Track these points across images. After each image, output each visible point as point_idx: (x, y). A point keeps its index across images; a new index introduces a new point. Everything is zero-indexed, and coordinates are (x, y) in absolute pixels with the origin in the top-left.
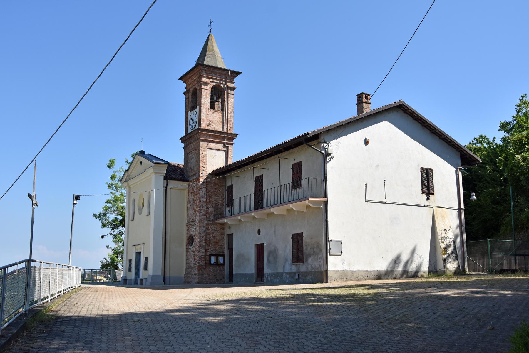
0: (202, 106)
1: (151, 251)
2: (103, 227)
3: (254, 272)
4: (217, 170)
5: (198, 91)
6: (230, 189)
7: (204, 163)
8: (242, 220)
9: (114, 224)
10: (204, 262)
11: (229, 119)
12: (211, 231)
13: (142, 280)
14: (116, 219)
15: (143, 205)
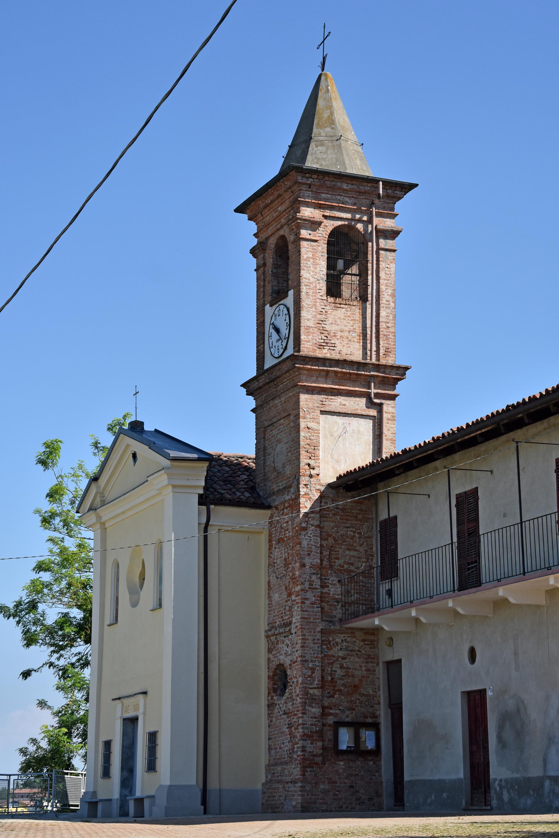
0: (304, 289)
1: (164, 715)
2: (28, 645)
3: (461, 776)
4: (349, 473)
5: (291, 247)
6: (389, 528)
7: (313, 455)
8: (423, 620)
9: (62, 635)
10: (320, 744)
11: (382, 325)
12: (336, 651)
13: (140, 801)
14: (65, 619)
15: (142, 578)
